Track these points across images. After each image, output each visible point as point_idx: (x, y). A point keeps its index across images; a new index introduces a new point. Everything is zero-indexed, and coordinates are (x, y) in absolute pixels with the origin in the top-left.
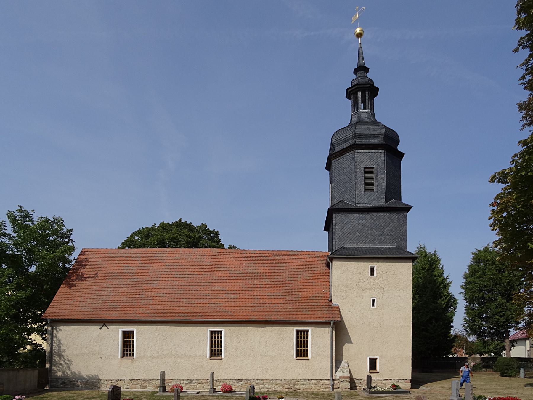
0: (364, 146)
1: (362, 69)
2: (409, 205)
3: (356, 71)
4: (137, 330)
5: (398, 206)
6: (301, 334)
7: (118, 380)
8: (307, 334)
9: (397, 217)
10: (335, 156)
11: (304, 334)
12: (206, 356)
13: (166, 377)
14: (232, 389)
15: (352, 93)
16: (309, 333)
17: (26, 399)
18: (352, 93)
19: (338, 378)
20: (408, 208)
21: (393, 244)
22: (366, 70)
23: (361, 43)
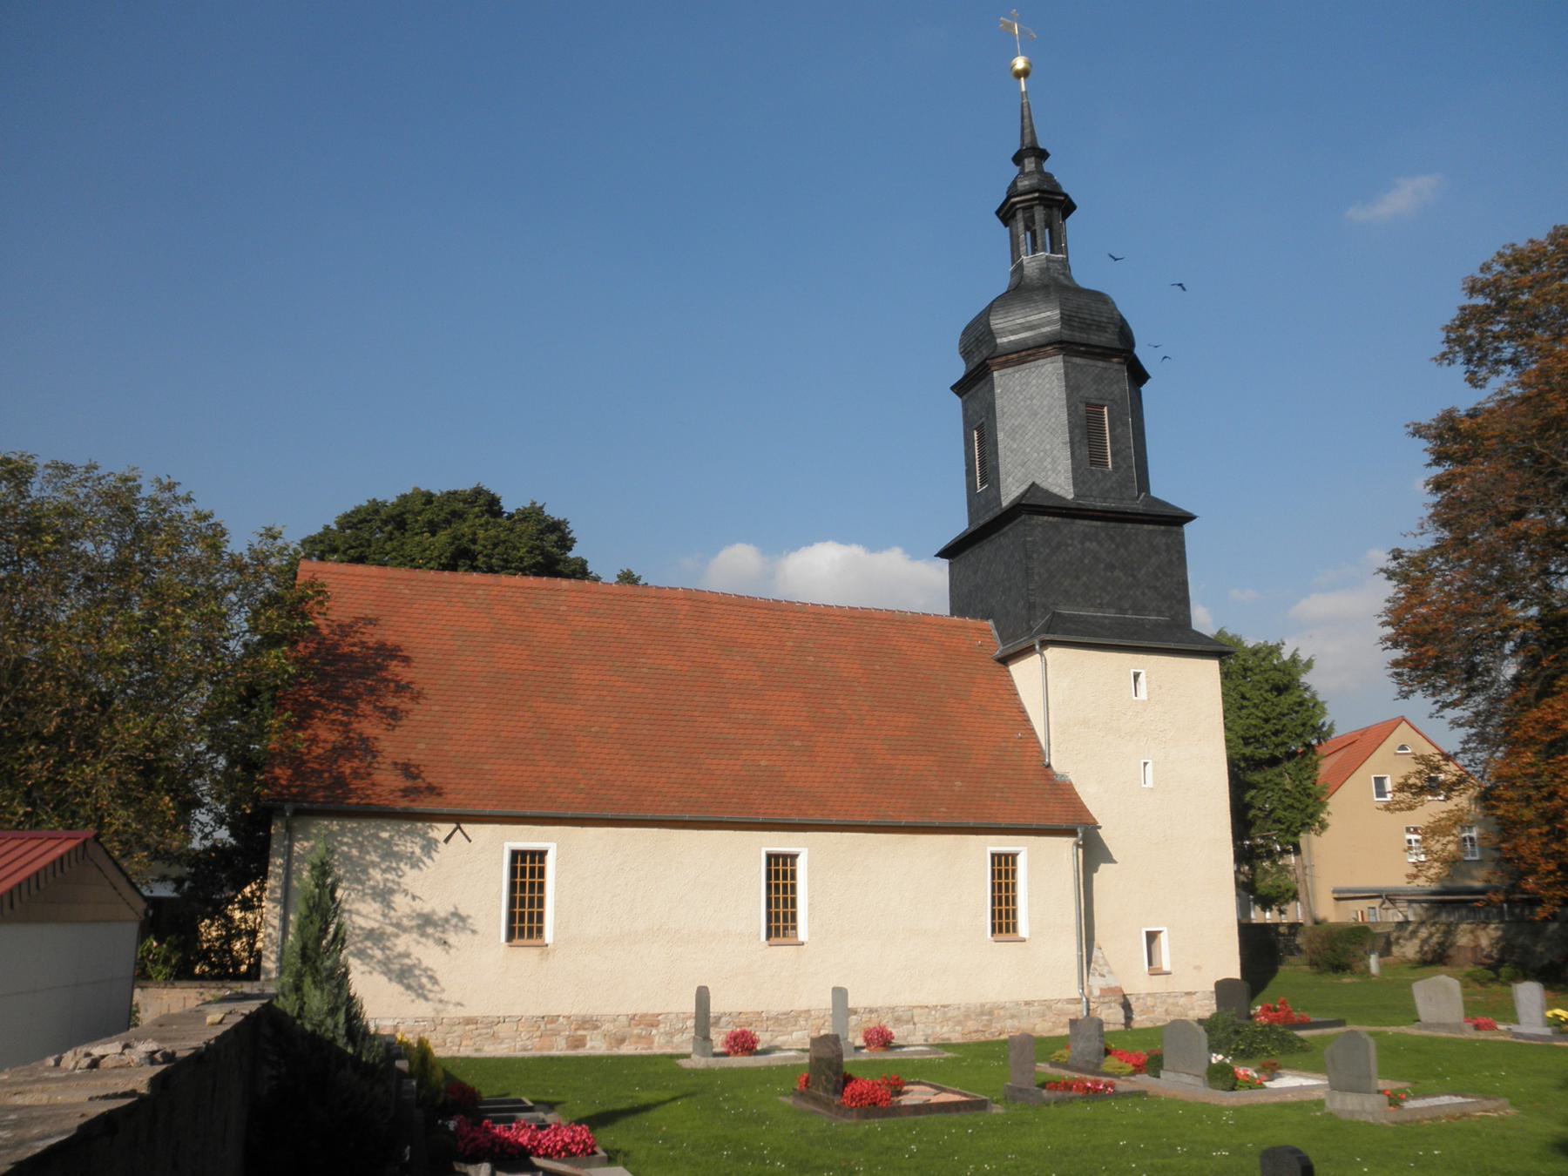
0: (1082, 349)
1: (1032, 152)
2: (1188, 513)
3: (1018, 159)
4: (558, 847)
5: (1138, 506)
6: (524, 861)
7: (497, 1020)
8: (542, 860)
9: (1164, 540)
10: (1006, 362)
11: (532, 861)
12: (759, 934)
13: (715, 1007)
14: (754, 1042)
15: (1018, 206)
16: (1022, 862)
17: (1207, 1063)
18: (1018, 206)
19: (1096, 992)
20: (1178, 519)
21: (1160, 613)
22: (1042, 155)
23: (1026, 92)
